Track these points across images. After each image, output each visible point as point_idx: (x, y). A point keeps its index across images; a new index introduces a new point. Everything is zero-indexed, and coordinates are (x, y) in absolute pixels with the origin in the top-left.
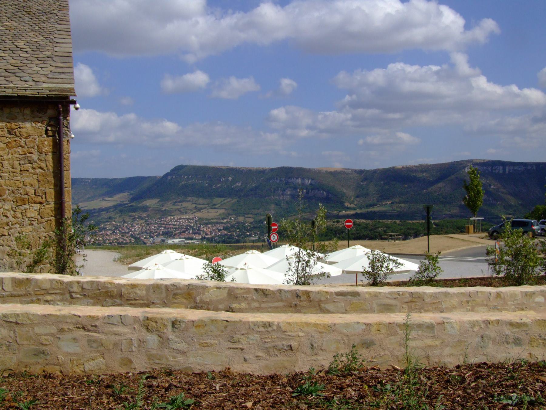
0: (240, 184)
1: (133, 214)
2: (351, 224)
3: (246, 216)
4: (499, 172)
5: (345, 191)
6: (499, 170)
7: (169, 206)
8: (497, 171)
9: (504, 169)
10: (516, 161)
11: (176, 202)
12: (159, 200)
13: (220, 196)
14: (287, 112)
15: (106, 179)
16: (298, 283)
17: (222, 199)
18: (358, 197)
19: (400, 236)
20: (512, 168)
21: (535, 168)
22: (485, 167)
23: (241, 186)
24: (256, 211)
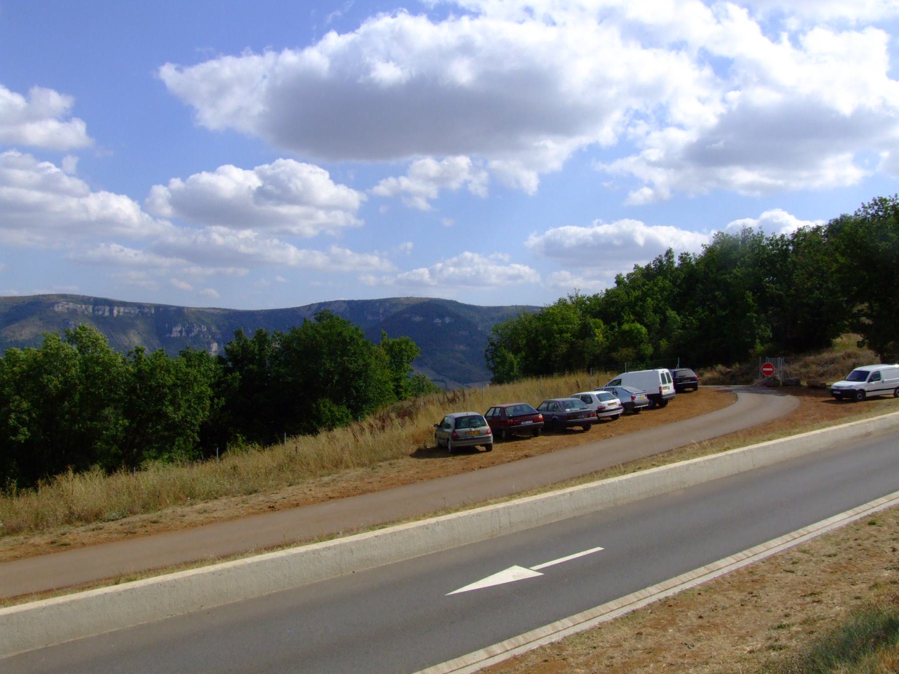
2: (764, 369)
4: (104, 313)
6: (104, 312)
8: (100, 313)
9: (111, 311)
10: (128, 300)
14: (857, 161)
15: (516, 306)
16: (704, 373)
19: (765, 372)
20: (122, 309)
21: (153, 311)
22: (84, 306)
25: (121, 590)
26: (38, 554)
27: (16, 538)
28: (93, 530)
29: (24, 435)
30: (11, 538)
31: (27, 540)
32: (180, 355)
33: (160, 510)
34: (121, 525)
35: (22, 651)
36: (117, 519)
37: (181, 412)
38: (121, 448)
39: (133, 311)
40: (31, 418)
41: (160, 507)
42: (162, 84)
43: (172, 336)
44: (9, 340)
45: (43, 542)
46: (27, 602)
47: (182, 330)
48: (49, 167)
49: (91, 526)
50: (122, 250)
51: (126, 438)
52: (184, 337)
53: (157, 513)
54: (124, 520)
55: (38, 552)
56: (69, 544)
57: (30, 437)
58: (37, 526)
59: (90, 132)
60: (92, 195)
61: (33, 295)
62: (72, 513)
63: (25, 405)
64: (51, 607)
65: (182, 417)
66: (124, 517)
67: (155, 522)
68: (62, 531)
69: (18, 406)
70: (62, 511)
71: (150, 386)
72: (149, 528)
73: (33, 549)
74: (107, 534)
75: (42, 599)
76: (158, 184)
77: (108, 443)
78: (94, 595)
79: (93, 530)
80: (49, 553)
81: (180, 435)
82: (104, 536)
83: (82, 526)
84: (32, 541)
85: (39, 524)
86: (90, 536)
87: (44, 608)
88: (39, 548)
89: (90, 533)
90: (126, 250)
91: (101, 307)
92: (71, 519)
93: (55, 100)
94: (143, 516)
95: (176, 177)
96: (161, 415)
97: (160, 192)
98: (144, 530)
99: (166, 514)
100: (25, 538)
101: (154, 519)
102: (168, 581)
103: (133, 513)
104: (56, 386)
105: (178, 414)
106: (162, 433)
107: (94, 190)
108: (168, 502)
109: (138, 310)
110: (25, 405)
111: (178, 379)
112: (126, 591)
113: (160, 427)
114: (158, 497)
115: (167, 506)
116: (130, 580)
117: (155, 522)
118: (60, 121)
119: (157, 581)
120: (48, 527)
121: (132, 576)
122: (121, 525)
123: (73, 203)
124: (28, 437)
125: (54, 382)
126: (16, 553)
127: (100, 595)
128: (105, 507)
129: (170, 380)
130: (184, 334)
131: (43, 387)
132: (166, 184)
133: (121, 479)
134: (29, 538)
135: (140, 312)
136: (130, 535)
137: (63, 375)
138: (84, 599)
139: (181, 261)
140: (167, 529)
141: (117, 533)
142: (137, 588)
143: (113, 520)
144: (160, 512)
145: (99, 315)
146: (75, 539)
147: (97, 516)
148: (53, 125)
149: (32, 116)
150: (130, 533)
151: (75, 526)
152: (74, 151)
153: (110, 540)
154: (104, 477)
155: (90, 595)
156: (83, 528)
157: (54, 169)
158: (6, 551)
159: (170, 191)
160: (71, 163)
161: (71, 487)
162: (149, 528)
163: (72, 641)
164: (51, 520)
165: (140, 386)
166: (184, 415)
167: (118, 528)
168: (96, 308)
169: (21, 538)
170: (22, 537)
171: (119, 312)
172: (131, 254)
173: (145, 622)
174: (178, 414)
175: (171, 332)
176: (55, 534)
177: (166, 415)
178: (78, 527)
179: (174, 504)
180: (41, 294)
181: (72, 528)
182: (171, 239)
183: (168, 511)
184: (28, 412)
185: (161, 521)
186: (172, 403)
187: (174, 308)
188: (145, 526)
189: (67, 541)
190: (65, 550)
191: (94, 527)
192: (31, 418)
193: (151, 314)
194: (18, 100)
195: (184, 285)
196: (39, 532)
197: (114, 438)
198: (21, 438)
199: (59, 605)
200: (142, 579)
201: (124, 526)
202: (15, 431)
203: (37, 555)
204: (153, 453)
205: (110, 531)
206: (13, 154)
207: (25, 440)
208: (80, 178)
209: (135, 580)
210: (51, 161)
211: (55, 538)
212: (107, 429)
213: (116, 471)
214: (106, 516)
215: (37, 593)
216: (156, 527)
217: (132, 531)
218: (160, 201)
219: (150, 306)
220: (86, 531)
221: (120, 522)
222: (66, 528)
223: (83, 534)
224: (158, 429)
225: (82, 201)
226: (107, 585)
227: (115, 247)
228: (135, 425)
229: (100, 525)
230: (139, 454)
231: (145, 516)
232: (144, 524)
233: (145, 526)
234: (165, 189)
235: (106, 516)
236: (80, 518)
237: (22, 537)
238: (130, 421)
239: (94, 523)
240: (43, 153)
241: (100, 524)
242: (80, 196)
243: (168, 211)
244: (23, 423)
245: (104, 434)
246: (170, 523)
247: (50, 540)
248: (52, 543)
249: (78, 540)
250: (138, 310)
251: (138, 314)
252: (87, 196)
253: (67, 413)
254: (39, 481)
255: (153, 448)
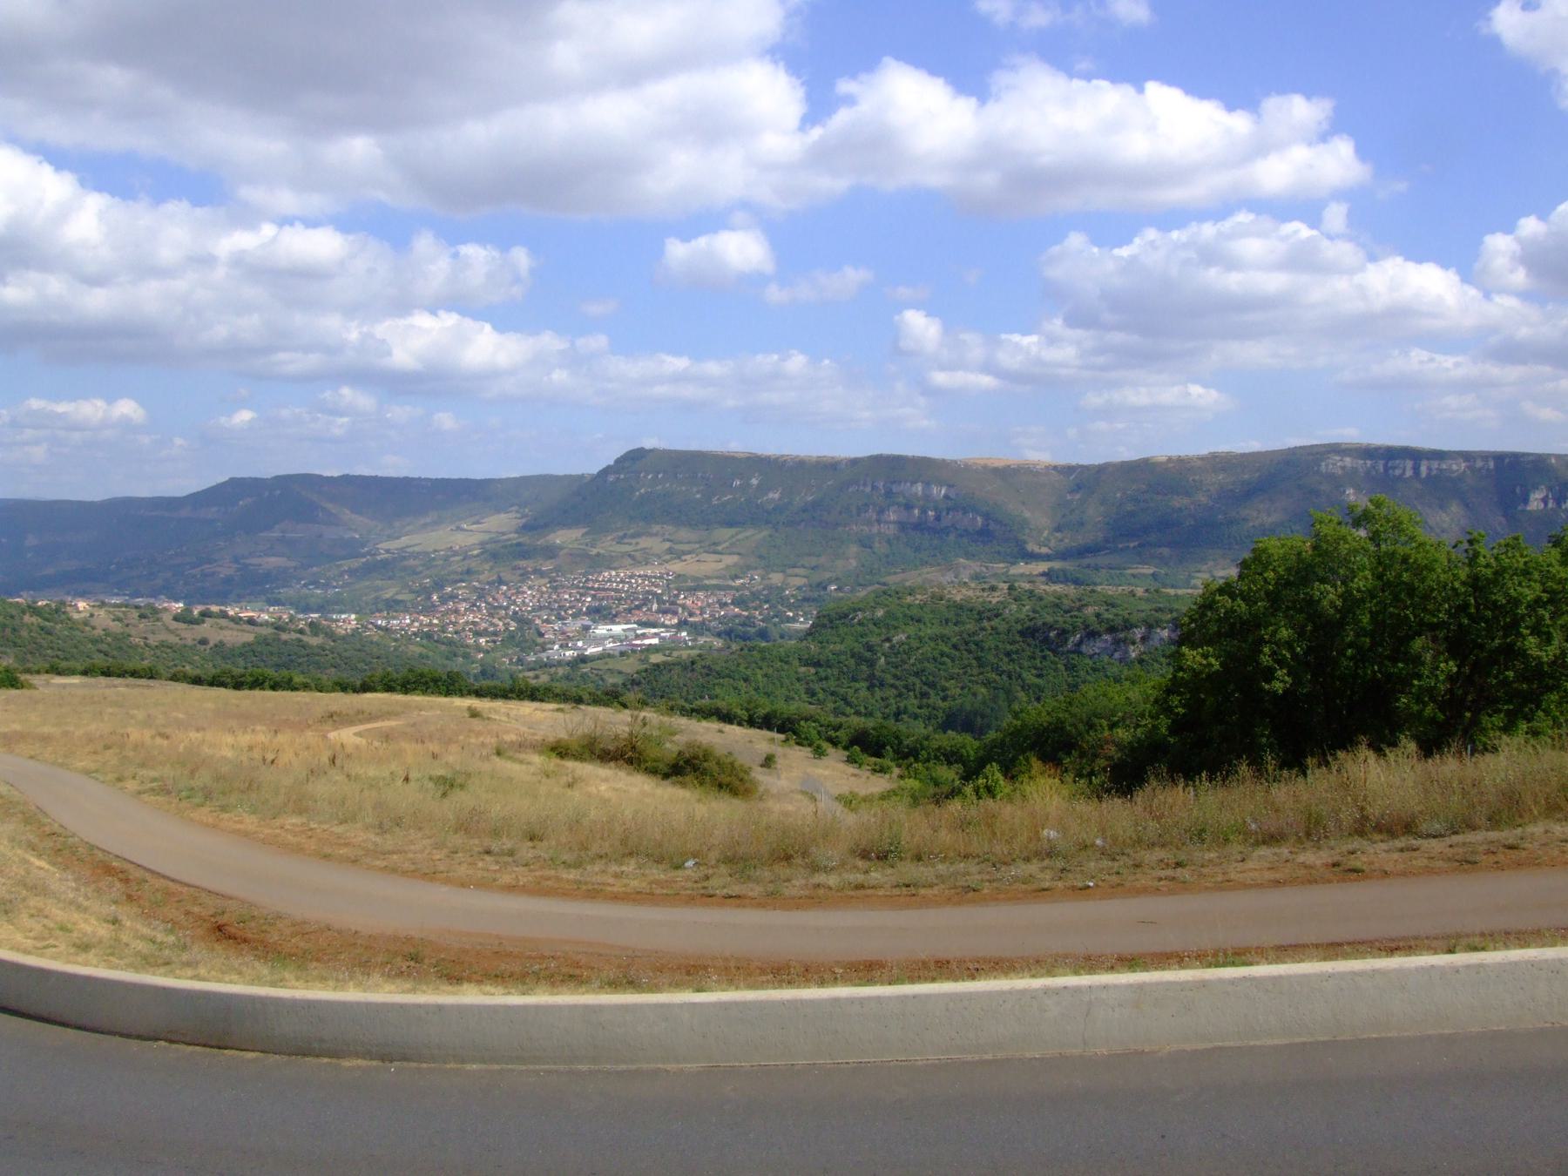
0: (777, 496)
1: (523, 563)
3: (789, 571)
5: (1027, 514)
6: (1404, 470)
7: (606, 545)
8: (1398, 472)
9: (1416, 469)
11: (625, 536)
12: (585, 530)
13: (730, 525)
17: (732, 531)
18: (1058, 529)
20: (1435, 465)
21: (1491, 464)
23: (779, 500)
24: (814, 561)
25: (1460, 963)
26: (1312, 881)
27: (1276, 850)
28: (1402, 850)
29: (1280, 683)
30: (1269, 851)
31: (1294, 856)
32: (1549, 542)
33: (1520, 826)
34: (1451, 846)
35: (1298, 1040)
36: (1442, 836)
37: (1553, 647)
38: (1442, 710)
39: (1455, 467)
40: (1295, 656)
41: (1519, 821)
42: (1495, 42)
43: (1528, 508)
44: (1251, 524)
45: (1318, 862)
46: (1302, 961)
47: (1547, 496)
48: (1296, 232)
49: (1399, 843)
50: (1432, 360)
51: (1450, 691)
52: (1552, 509)
53: (1515, 831)
54: (1455, 839)
55: (1310, 878)
56: (1363, 871)
57: (1291, 685)
58: (1308, 835)
59: (1362, 152)
60: (1370, 266)
61: (1120, 460)
62: (1365, 818)
63: (1285, 633)
64: (1342, 976)
65: (1555, 656)
66: (1456, 833)
67: (1511, 847)
68: (1350, 847)
69: (1275, 632)
70: (1348, 815)
71: (1495, 602)
72: (1500, 857)
73: (1303, 872)
74: (1426, 861)
75: (1325, 959)
76: (1493, 232)
77: (1419, 700)
78: (1413, 965)
79: (1402, 850)
80: (1330, 881)
81: (1550, 689)
82: (1420, 862)
83: (1382, 841)
84: (1301, 858)
85: (1312, 830)
86: (1396, 861)
87: (1330, 976)
88: (1314, 872)
89: (1396, 856)
90: (1439, 358)
91: (1397, 462)
92: (1363, 827)
93: (1301, 110)
94: (1490, 833)
95: (1527, 215)
96: (1511, 652)
97: (1500, 245)
98: (1492, 858)
99: (1533, 834)
100: (1291, 852)
101: (1511, 841)
102: (1546, 961)
103: (1473, 828)
104: (1332, 602)
105: (1546, 651)
106: (1515, 685)
107: (1373, 258)
108: (1536, 812)
109: (1463, 465)
110: (1285, 633)
111: (1544, 591)
112: (1468, 967)
113: (1511, 674)
114: (1517, 802)
115: (1534, 820)
116: (1475, 949)
117: (1511, 847)
118: (1310, 144)
119: (1526, 958)
120: (1326, 837)
121: (1477, 941)
122: (1451, 846)
123: (1341, 284)
124: (1288, 686)
125: (1329, 595)
126: (1278, 876)
127: (1422, 968)
128: (1421, 812)
129: (1530, 592)
130: (1550, 505)
131: (1311, 602)
132: (1509, 228)
133: (1448, 766)
134: (1296, 853)
135: (1468, 467)
136: (1466, 866)
137: (1344, 583)
138: (1395, 970)
139: (1547, 369)
140: (1534, 863)
141: (1443, 859)
142: (1488, 966)
143: (1435, 837)
144: (1520, 829)
145: (1394, 476)
146: (1371, 863)
147: (1408, 827)
148: (1300, 154)
149: (1261, 148)
150: (1467, 863)
151: (1369, 839)
152: (1339, 195)
153: (1429, 871)
154: (1419, 760)
155: (1407, 965)
156: (1384, 846)
157: (1305, 232)
158: (1261, 869)
159: (1519, 240)
160: (1336, 215)
161: (1362, 774)
162: (1500, 857)
163: (1376, 1039)
164: (1331, 825)
165: (1476, 601)
166: (1558, 652)
167: (1445, 851)
168: (1390, 464)
169: (1284, 851)
170: (1286, 851)
171: (1429, 469)
172: (1450, 365)
173: (1503, 1028)
174: (1546, 651)
175: (1526, 501)
176: (1338, 851)
177: (1523, 654)
178: (1375, 842)
179: (1547, 817)
180: (1298, 445)
181: (1365, 843)
182: (1524, 332)
183: (1537, 829)
184: (1289, 645)
185: (1522, 846)
186: (1536, 630)
187: (1531, 458)
188: (1493, 853)
189: (1358, 864)
190: (1355, 880)
191: (1403, 845)
192: (1295, 656)
193: (1488, 469)
194: (1240, 123)
195: (1547, 414)
196: (1312, 844)
197: (1430, 691)
198: (1278, 687)
199: (1355, 974)
200: (1495, 949)
201: (1455, 850)
202: (1269, 675)
203: (1310, 882)
204: (1498, 720)
205: (1432, 855)
206: (1243, 218)
207: (1284, 691)
208: (1350, 239)
209: (1483, 949)
210: (1302, 219)
211: (1337, 858)
212: (1419, 677)
213: (1439, 749)
214: (1424, 827)
215: (1317, 946)
216: (1514, 857)
217: (1470, 859)
218: (1500, 262)
219: (1485, 456)
220: (1387, 851)
221: (1448, 841)
222: (1356, 843)
223: (1384, 854)
224: (1507, 677)
225: (1358, 279)
226: (1435, 951)
227: (1418, 356)
228: (1467, 670)
229: (1415, 842)
230: (1475, 722)
231: (1493, 835)
232: (1492, 849)
233: (1493, 853)
234: (1509, 238)
235: (1424, 827)
236: (1379, 828)
237: (1286, 851)
238: (1458, 662)
239: (1403, 839)
240: (1280, 208)
241: (1414, 842)
242: (1352, 272)
243: (1520, 277)
244: (1281, 663)
245: (1414, 686)
246: (1540, 852)
247: (1330, 861)
248: (1334, 865)
249: (1377, 865)
250: (1463, 465)
251: (1465, 471)
252: (1362, 269)
253: (1350, 645)
254: (1309, 760)
255: (1498, 711)
